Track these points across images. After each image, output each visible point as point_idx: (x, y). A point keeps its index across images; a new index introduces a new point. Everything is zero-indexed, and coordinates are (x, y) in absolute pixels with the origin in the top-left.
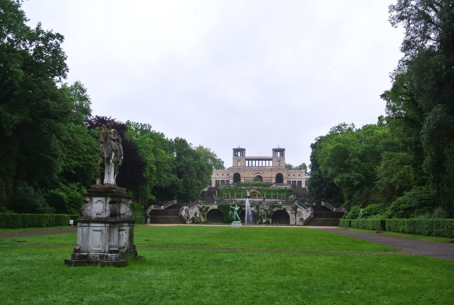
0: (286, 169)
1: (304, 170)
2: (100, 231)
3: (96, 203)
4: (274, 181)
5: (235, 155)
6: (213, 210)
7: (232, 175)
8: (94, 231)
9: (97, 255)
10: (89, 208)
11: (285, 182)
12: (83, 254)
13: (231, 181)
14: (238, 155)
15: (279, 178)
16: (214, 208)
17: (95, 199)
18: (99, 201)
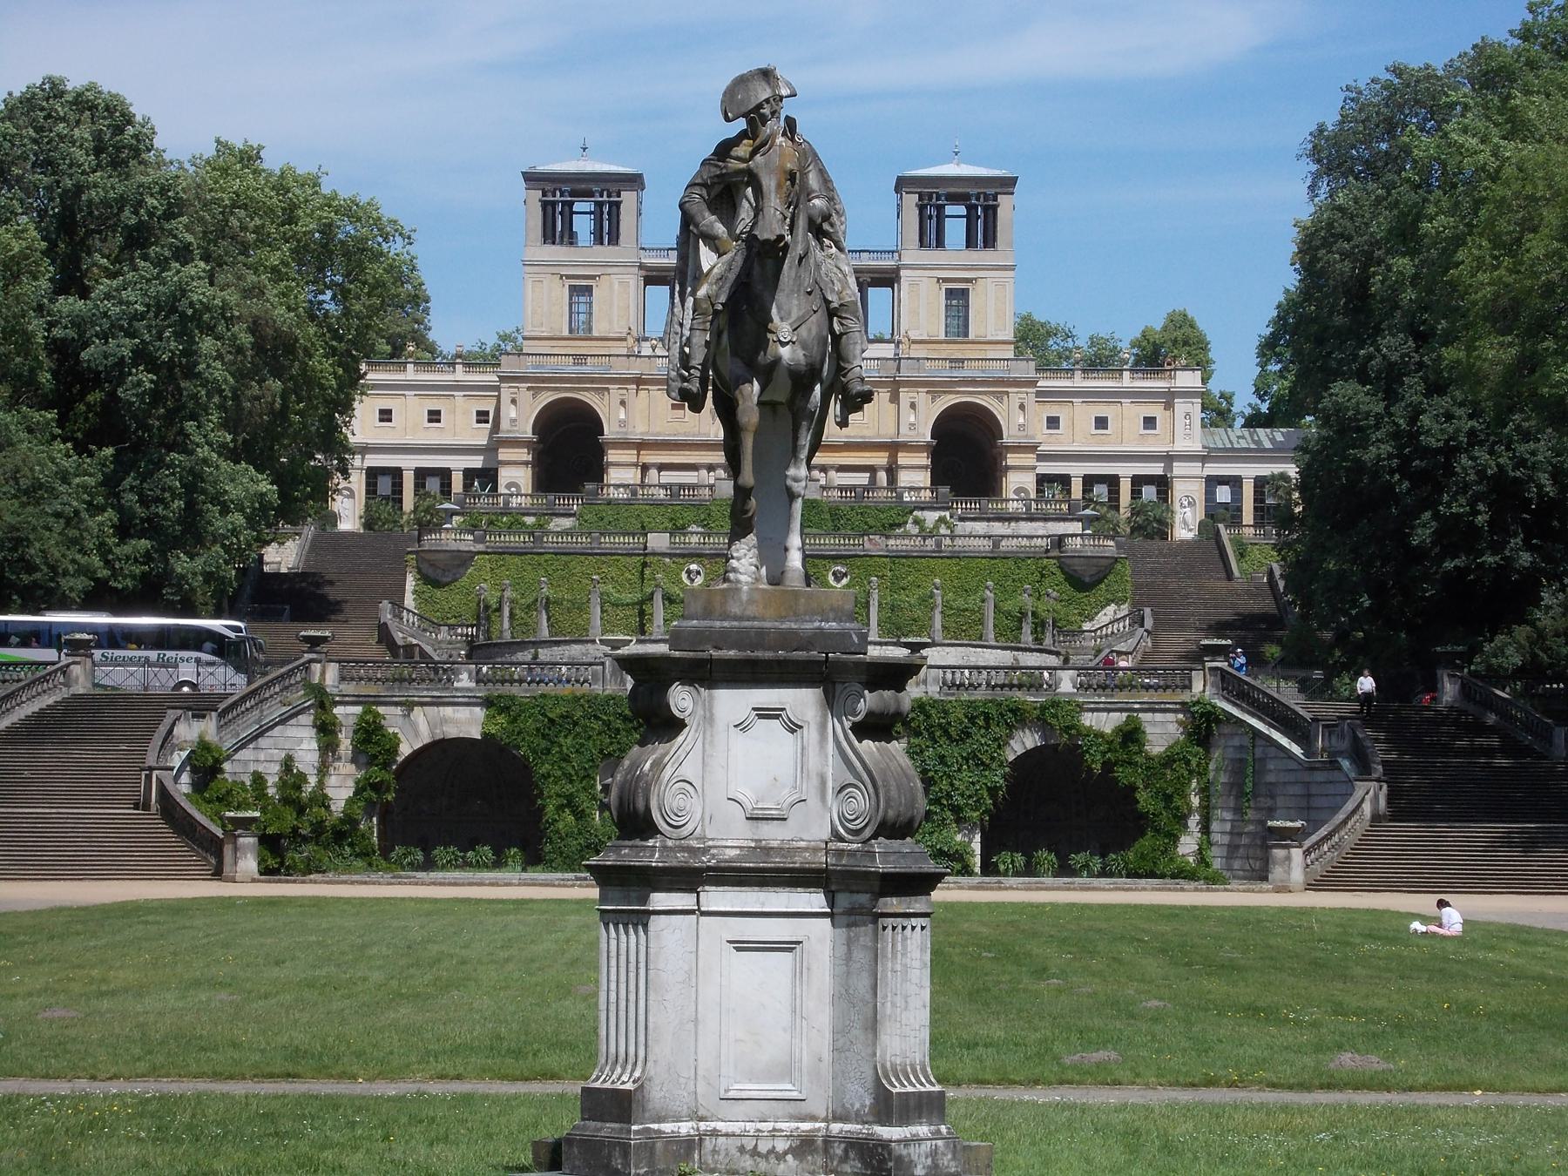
0: (1026, 369)
1: (1188, 380)
2: (788, 947)
3: (742, 727)
4: (916, 476)
5: (549, 236)
6: (442, 750)
7: (521, 415)
8: (741, 946)
9: (774, 1134)
10: (690, 770)
11: (1018, 481)
12: (667, 1127)
13: (517, 477)
14: (570, 238)
15: (967, 453)
16: (452, 732)
17: (733, 702)
18: (765, 714)
